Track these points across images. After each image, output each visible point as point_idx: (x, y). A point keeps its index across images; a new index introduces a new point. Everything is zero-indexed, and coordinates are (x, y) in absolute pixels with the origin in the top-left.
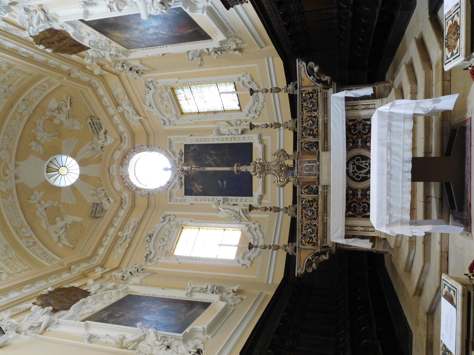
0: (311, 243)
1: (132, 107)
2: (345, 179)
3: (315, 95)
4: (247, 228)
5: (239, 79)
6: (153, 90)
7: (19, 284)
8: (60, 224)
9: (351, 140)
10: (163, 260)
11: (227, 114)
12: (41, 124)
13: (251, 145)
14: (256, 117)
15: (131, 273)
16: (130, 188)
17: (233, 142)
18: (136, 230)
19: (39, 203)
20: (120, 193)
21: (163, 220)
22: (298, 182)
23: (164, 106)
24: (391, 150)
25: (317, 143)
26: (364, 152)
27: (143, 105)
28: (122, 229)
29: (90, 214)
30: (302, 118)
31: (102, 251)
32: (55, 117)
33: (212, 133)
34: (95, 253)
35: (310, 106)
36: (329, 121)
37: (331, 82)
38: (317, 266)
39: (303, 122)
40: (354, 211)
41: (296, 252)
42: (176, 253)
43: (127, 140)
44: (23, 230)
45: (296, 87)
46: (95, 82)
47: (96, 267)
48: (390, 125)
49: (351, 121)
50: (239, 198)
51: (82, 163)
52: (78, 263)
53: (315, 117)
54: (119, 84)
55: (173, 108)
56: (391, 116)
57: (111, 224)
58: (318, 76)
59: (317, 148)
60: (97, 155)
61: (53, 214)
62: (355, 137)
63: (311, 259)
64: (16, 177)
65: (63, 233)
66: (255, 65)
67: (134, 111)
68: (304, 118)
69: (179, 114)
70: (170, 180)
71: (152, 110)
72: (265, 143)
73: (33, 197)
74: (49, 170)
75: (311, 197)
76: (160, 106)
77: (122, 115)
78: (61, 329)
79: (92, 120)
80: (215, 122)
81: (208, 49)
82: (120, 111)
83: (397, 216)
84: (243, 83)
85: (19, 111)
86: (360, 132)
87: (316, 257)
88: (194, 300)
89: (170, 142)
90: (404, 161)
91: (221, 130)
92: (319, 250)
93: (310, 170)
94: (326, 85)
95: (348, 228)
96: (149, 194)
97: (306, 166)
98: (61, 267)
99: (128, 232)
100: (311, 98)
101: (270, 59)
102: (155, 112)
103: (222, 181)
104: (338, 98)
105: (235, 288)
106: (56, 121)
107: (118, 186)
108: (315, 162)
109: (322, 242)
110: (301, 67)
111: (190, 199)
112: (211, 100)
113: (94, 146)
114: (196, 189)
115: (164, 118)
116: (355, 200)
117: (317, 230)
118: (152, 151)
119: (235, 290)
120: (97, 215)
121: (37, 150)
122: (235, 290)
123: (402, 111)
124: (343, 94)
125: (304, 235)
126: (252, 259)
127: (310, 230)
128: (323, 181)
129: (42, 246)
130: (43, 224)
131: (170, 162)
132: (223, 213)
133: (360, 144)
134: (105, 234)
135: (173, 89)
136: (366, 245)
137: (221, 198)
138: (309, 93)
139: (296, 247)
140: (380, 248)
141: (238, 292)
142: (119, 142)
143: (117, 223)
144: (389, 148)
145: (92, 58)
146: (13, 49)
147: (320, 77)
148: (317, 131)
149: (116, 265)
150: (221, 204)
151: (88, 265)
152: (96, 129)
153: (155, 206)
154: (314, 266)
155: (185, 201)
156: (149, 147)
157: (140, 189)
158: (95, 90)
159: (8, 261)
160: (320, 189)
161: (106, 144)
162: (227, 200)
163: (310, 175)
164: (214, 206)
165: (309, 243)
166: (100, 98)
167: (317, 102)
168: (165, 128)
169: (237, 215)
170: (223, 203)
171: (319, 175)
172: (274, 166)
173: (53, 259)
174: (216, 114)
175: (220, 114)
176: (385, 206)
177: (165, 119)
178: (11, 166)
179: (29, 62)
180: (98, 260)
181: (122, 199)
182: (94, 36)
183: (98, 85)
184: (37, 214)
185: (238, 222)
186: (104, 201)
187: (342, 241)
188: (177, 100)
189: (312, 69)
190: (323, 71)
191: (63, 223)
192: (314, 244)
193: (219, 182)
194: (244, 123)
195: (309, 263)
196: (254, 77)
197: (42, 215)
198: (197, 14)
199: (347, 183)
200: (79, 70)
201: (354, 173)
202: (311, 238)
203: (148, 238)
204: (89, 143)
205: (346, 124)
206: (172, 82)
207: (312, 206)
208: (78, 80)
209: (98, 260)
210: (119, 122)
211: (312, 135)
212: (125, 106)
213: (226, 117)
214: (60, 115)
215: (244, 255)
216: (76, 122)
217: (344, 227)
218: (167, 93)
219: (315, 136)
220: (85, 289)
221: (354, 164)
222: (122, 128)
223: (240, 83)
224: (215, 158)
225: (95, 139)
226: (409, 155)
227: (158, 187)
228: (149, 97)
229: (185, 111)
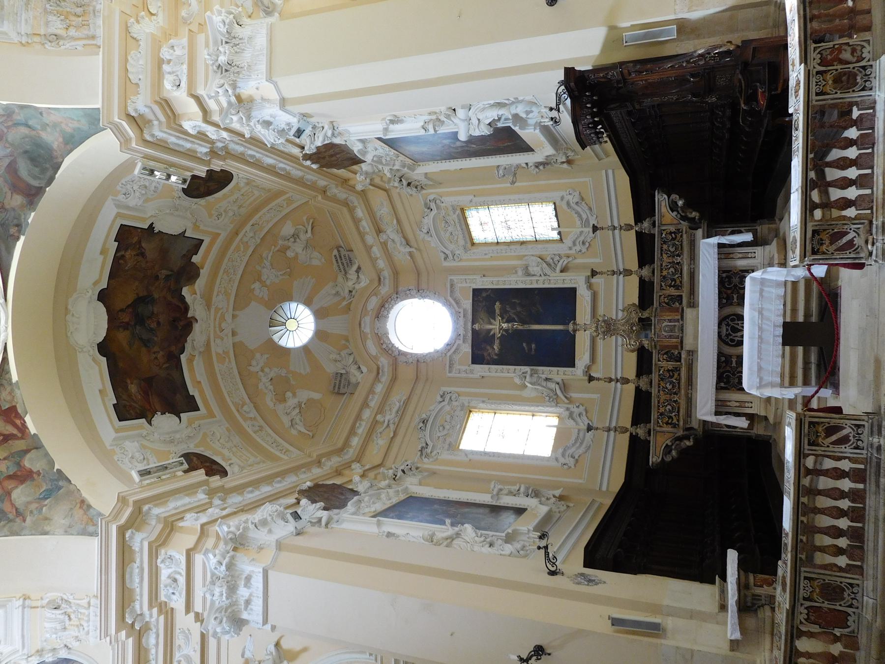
0: (671, 424)
1: (401, 235)
2: (716, 343)
3: (679, 236)
4: (567, 413)
5: (562, 198)
6: (435, 211)
7: (287, 469)
8: (292, 402)
9: (725, 296)
10: (445, 456)
11: (540, 246)
12: (269, 258)
13: (573, 291)
14: (584, 250)
15: (403, 471)
16: (390, 352)
17: (546, 286)
18: (402, 412)
19: (262, 371)
20: (375, 359)
21: (441, 400)
22: (655, 346)
23: (448, 234)
24: (762, 315)
25: (681, 296)
26: (737, 310)
27: (418, 232)
28: (381, 410)
29: (331, 388)
30: (661, 265)
31: (355, 441)
32: (289, 247)
33: (516, 272)
34: (346, 444)
35: (672, 250)
36: (696, 270)
37: (700, 219)
38: (677, 453)
39: (662, 269)
40: (727, 383)
41: (650, 435)
42: (461, 447)
43: (387, 281)
44: (245, 408)
45: (654, 225)
46: (354, 200)
47: (353, 461)
48: (761, 291)
49: (724, 272)
50: (555, 369)
51: (319, 315)
52: (329, 455)
53: (678, 263)
54: (386, 203)
55: (461, 236)
56: (763, 282)
57: (365, 405)
58: (683, 212)
59: (681, 304)
60: (345, 303)
61: (283, 387)
62: (729, 292)
63: (670, 444)
64: (234, 334)
65: (297, 415)
66: (587, 179)
67: (403, 240)
68: (664, 264)
69: (469, 244)
70: (450, 340)
71: (429, 239)
72: (595, 288)
73: (254, 363)
74: (272, 323)
75: (670, 365)
76: (442, 233)
77: (384, 245)
78: (345, 526)
79: (339, 251)
80: (521, 258)
81: (527, 164)
82: (382, 240)
83: (768, 379)
84: (568, 203)
85: (245, 239)
86: (735, 286)
87: (677, 442)
88: (502, 504)
89: (452, 286)
90: (775, 326)
91: (530, 269)
92: (680, 433)
93: (671, 331)
94: (694, 225)
95: (720, 403)
96: (419, 362)
97: (666, 326)
98: (310, 460)
99: (390, 416)
100: (673, 239)
101: (610, 172)
102: (434, 242)
103: (529, 344)
104: (709, 244)
105: (557, 493)
106: (290, 254)
107: (373, 349)
108: (678, 321)
109: (685, 422)
110: (661, 200)
111: (481, 370)
112: (516, 223)
113: (338, 289)
114: (489, 355)
115: (445, 251)
116: (728, 368)
117: (679, 408)
118: (424, 297)
119: (557, 495)
120: (342, 391)
121: (261, 296)
122: (557, 495)
123: (774, 278)
124: (715, 240)
125: (662, 414)
126: (576, 457)
127: (669, 407)
128: (688, 344)
129: (270, 431)
130: (269, 400)
131: (451, 314)
132: (531, 391)
133: (735, 300)
134: (358, 417)
135: (462, 210)
136: (742, 423)
137: (527, 369)
138: (671, 233)
139: (650, 430)
140: (759, 430)
141: (561, 498)
142: (376, 283)
143: (374, 403)
144: (761, 312)
145: (367, 173)
146: (270, 165)
147: (685, 213)
148: (681, 282)
149: (377, 461)
150: (528, 377)
151: (339, 459)
152: (343, 264)
153: (427, 379)
154: (674, 453)
155: (472, 372)
156: (420, 290)
157: (405, 354)
158: (351, 210)
159: (234, 449)
160: (683, 356)
161: (357, 287)
162: (536, 372)
163: (670, 337)
164: (517, 381)
165: (667, 423)
166: (356, 221)
167: (681, 245)
168: (446, 264)
169: (552, 394)
170: (531, 375)
171: (682, 338)
172: (623, 325)
173: (287, 451)
174: (523, 246)
175: (530, 246)
176: (756, 369)
177: (447, 252)
178: (228, 317)
179: (255, 169)
180: (351, 453)
181: (378, 369)
182: (381, 151)
183: (356, 204)
184: (261, 386)
185: (553, 404)
186: (353, 370)
187: (712, 418)
188: (467, 225)
189: (676, 203)
190: (688, 205)
191: (296, 401)
192: (675, 426)
193: (524, 345)
194: (564, 258)
195: (668, 450)
196: (584, 196)
197: (266, 388)
198: (527, 131)
199: (718, 347)
200: (337, 186)
201: (728, 335)
202: (671, 417)
203: (421, 425)
204: (331, 284)
205: (719, 276)
206: (463, 200)
207: (672, 377)
208: (334, 199)
209: (351, 453)
210: (379, 255)
211: (674, 286)
212: (391, 233)
213: (539, 250)
214: (296, 244)
215: (565, 450)
216: (316, 254)
217: (714, 402)
218: (455, 216)
219: (677, 287)
220: (350, 487)
221: (728, 325)
222: (381, 264)
223: (565, 207)
224: (518, 309)
225: (340, 279)
226: (781, 320)
227: (432, 350)
228: (428, 222)
229: (475, 241)
